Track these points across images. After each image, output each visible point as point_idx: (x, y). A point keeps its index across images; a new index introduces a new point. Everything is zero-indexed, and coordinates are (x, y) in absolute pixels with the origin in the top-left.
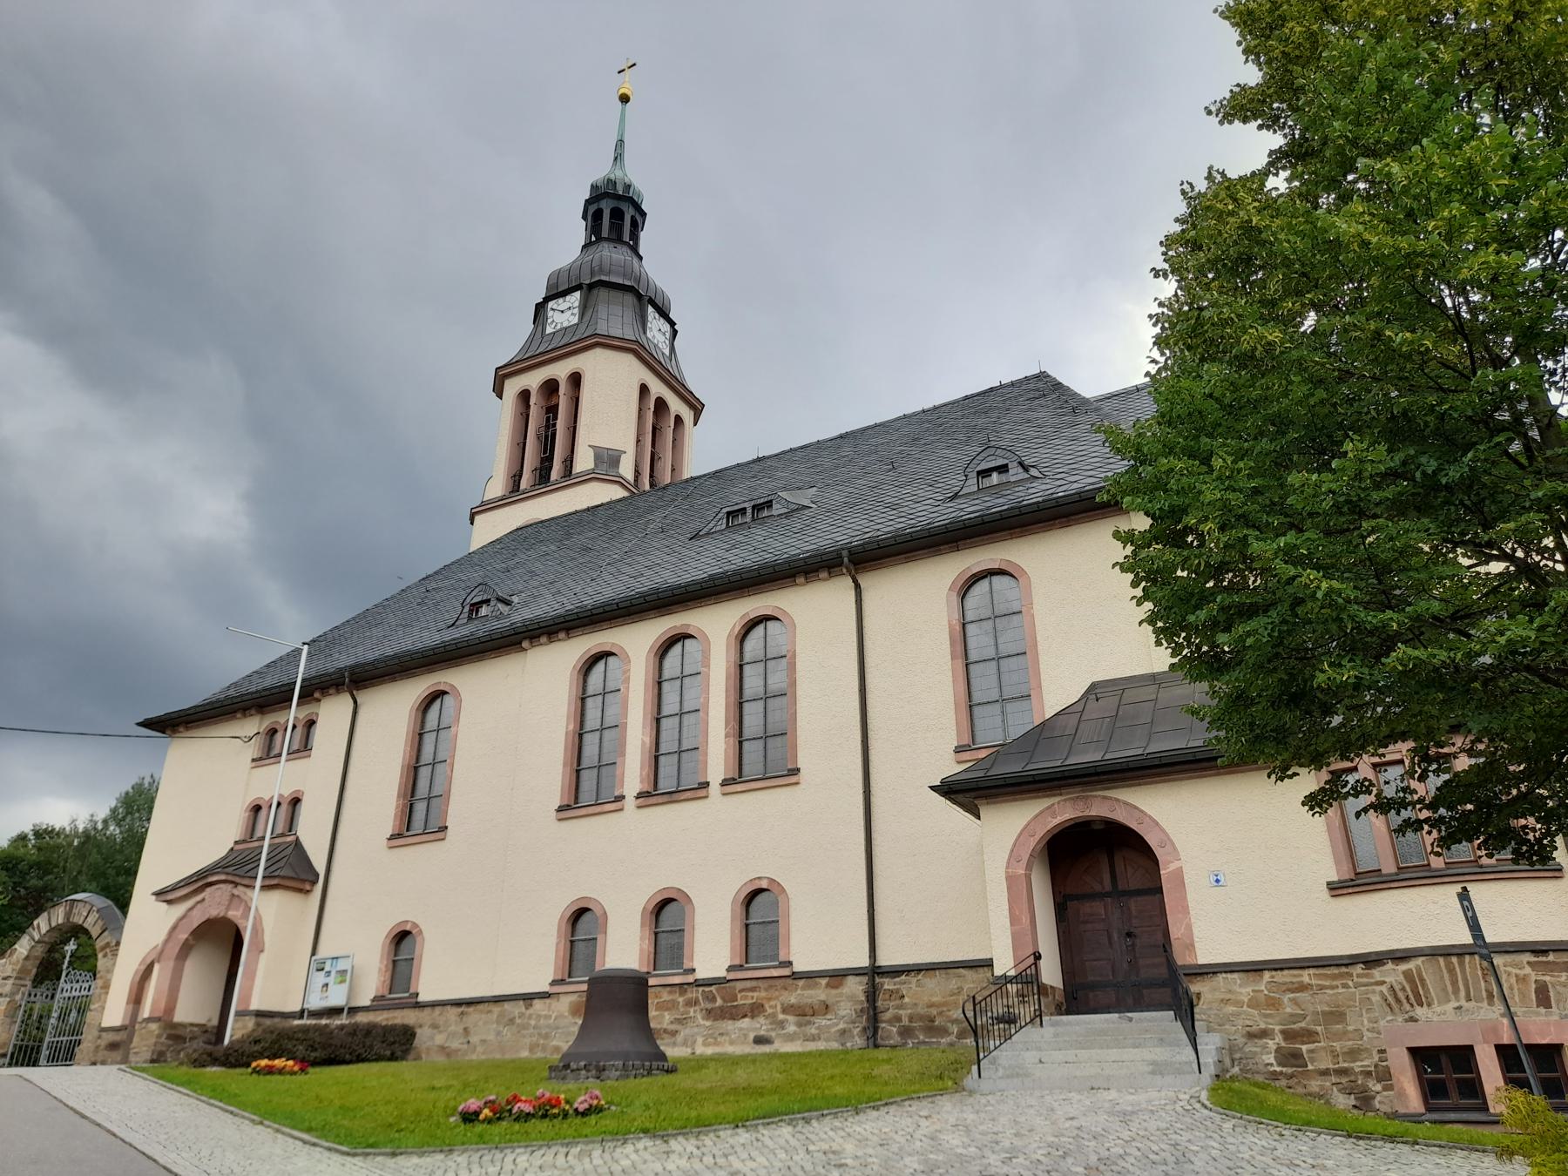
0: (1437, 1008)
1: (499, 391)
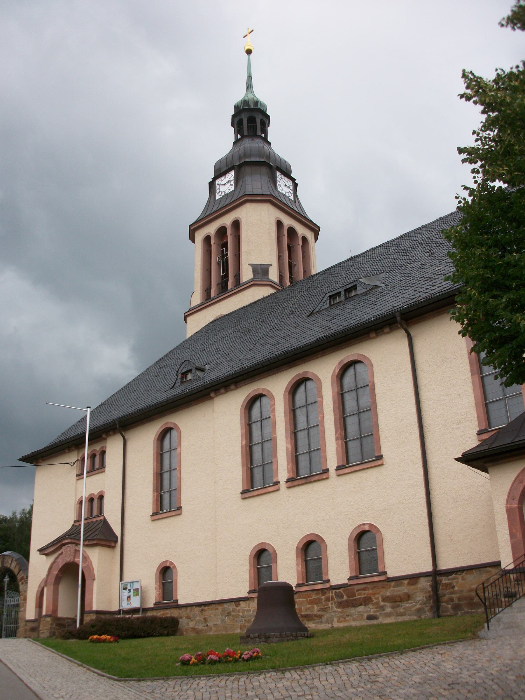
1: (192, 238)
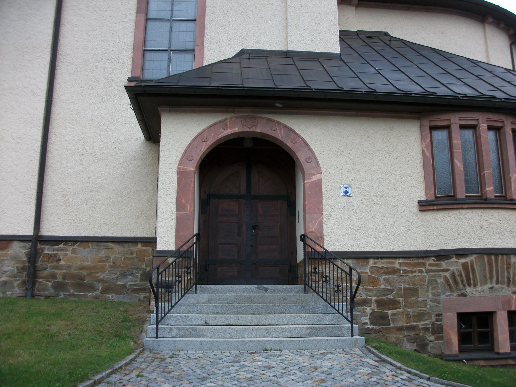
0: (479, 288)
